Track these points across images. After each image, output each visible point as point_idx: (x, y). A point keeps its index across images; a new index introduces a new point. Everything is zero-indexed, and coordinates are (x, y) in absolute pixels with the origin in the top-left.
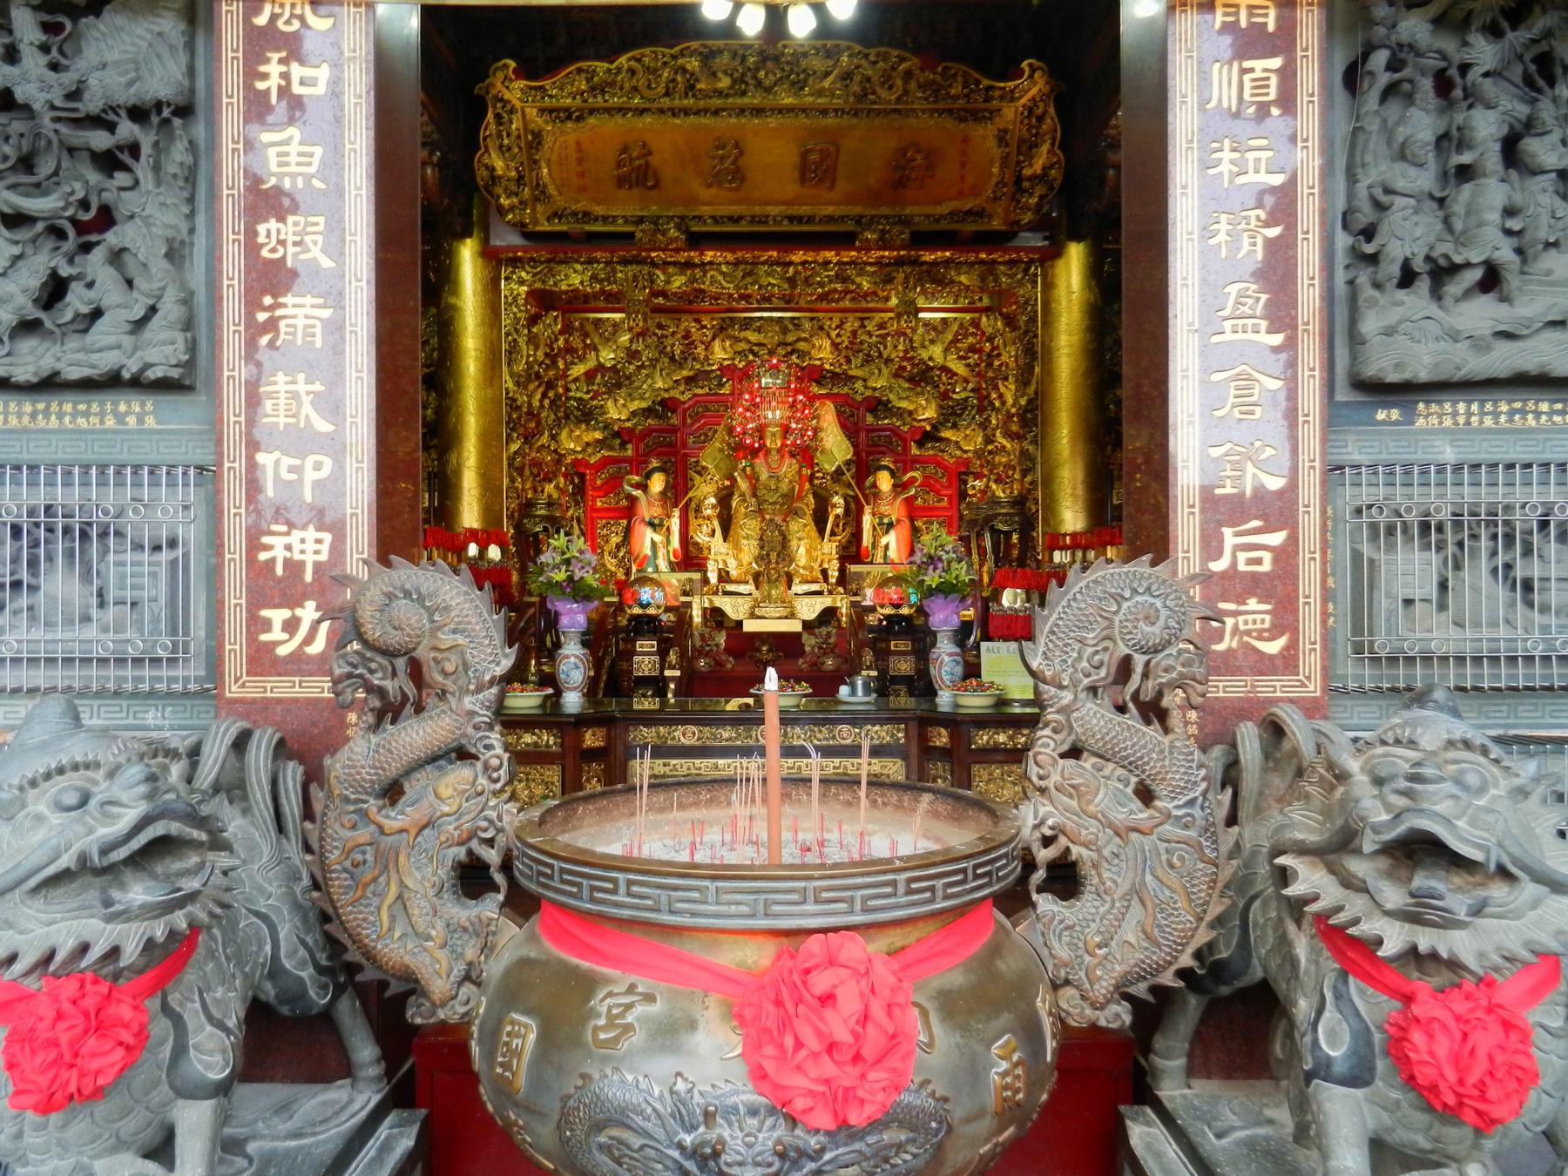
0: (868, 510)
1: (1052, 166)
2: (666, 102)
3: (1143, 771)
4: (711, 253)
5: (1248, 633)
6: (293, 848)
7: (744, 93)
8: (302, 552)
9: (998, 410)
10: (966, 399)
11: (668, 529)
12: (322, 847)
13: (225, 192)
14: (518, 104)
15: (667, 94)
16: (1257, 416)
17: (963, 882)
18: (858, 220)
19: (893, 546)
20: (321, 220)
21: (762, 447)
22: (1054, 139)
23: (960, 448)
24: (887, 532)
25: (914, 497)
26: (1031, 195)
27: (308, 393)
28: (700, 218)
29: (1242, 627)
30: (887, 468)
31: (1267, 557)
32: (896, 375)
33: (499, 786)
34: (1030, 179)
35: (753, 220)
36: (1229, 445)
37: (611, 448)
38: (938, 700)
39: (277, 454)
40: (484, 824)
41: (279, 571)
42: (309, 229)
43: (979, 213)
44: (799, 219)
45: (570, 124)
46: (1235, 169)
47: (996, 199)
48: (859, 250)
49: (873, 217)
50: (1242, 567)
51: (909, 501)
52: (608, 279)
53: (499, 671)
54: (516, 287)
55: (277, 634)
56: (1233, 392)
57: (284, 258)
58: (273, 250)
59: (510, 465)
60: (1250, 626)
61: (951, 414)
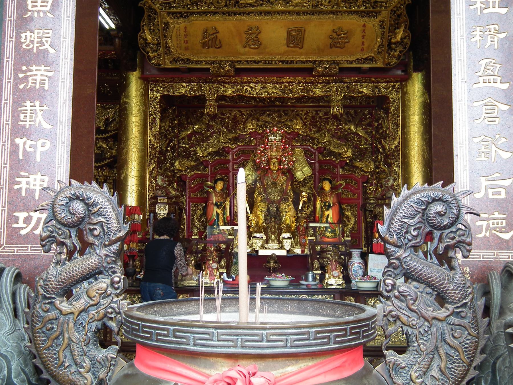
0: (319, 199)
1: (405, 38)
2: (226, 9)
3: (439, 289)
4: (245, 78)
5: (494, 229)
6: (22, 324)
7: (261, 5)
8: (35, 185)
9: (382, 154)
10: (366, 148)
11: (225, 207)
12: (33, 321)
13: (7, 19)
14: (158, 11)
15: (226, 6)
16: (497, 123)
17: (345, 335)
18: (314, 62)
19: (331, 216)
20: (50, 31)
21: (269, 168)
22: (406, 25)
23: (363, 171)
24: (328, 210)
25: (342, 193)
26: (395, 51)
27: (41, 110)
28: (241, 61)
29: (491, 226)
30: (328, 179)
31: (503, 191)
32: (333, 136)
33: (118, 291)
34: (395, 43)
35: (265, 62)
36: (483, 137)
37: (198, 170)
38: (352, 285)
39: (25, 139)
40: (110, 310)
41: (23, 194)
42: (45, 36)
43: (371, 60)
44: (287, 62)
45: (182, 20)
46: (483, 6)
47: (379, 53)
48: (314, 76)
49: (321, 61)
50: (490, 196)
51: (338, 195)
52: (198, 90)
53: (121, 234)
54: (155, 94)
55: (21, 224)
56: (484, 111)
57: (33, 48)
58: (28, 45)
59: (150, 175)
60: (496, 225)
61: (360, 154)
